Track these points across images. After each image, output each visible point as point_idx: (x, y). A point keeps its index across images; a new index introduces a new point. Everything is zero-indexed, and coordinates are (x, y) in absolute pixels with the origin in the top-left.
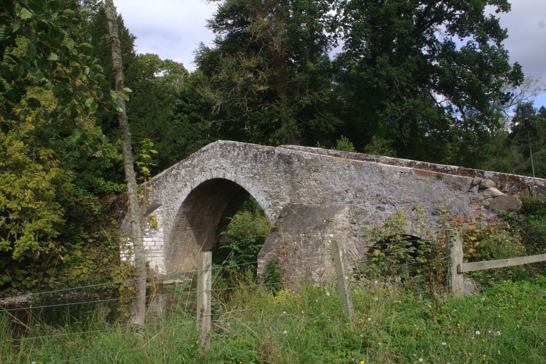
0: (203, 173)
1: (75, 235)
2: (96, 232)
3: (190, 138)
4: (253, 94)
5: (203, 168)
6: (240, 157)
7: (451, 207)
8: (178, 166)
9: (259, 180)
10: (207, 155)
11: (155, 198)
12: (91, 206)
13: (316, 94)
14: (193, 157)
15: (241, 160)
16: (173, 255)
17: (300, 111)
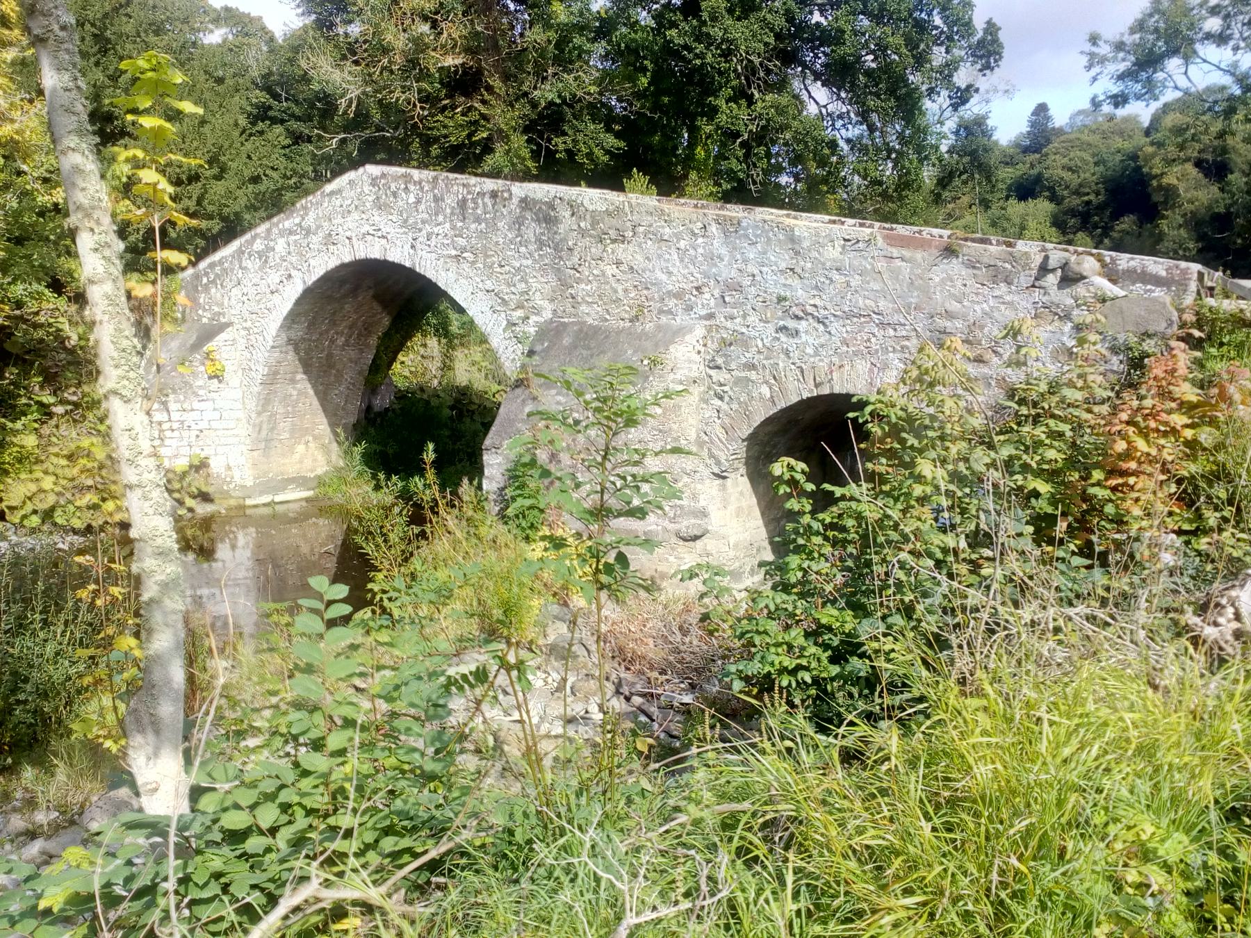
0: (331, 247)
1: (20, 396)
2: (73, 389)
3: (288, 174)
4: (429, 75)
5: (330, 235)
6: (422, 207)
7: (982, 327)
8: (269, 231)
9: (473, 263)
10: (338, 203)
11: (216, 309)
12: (60, 326)
13: (570, 78)
14: (305, 208)
15: (425, 216)
16: (268, 440)
17: (534, 116)
